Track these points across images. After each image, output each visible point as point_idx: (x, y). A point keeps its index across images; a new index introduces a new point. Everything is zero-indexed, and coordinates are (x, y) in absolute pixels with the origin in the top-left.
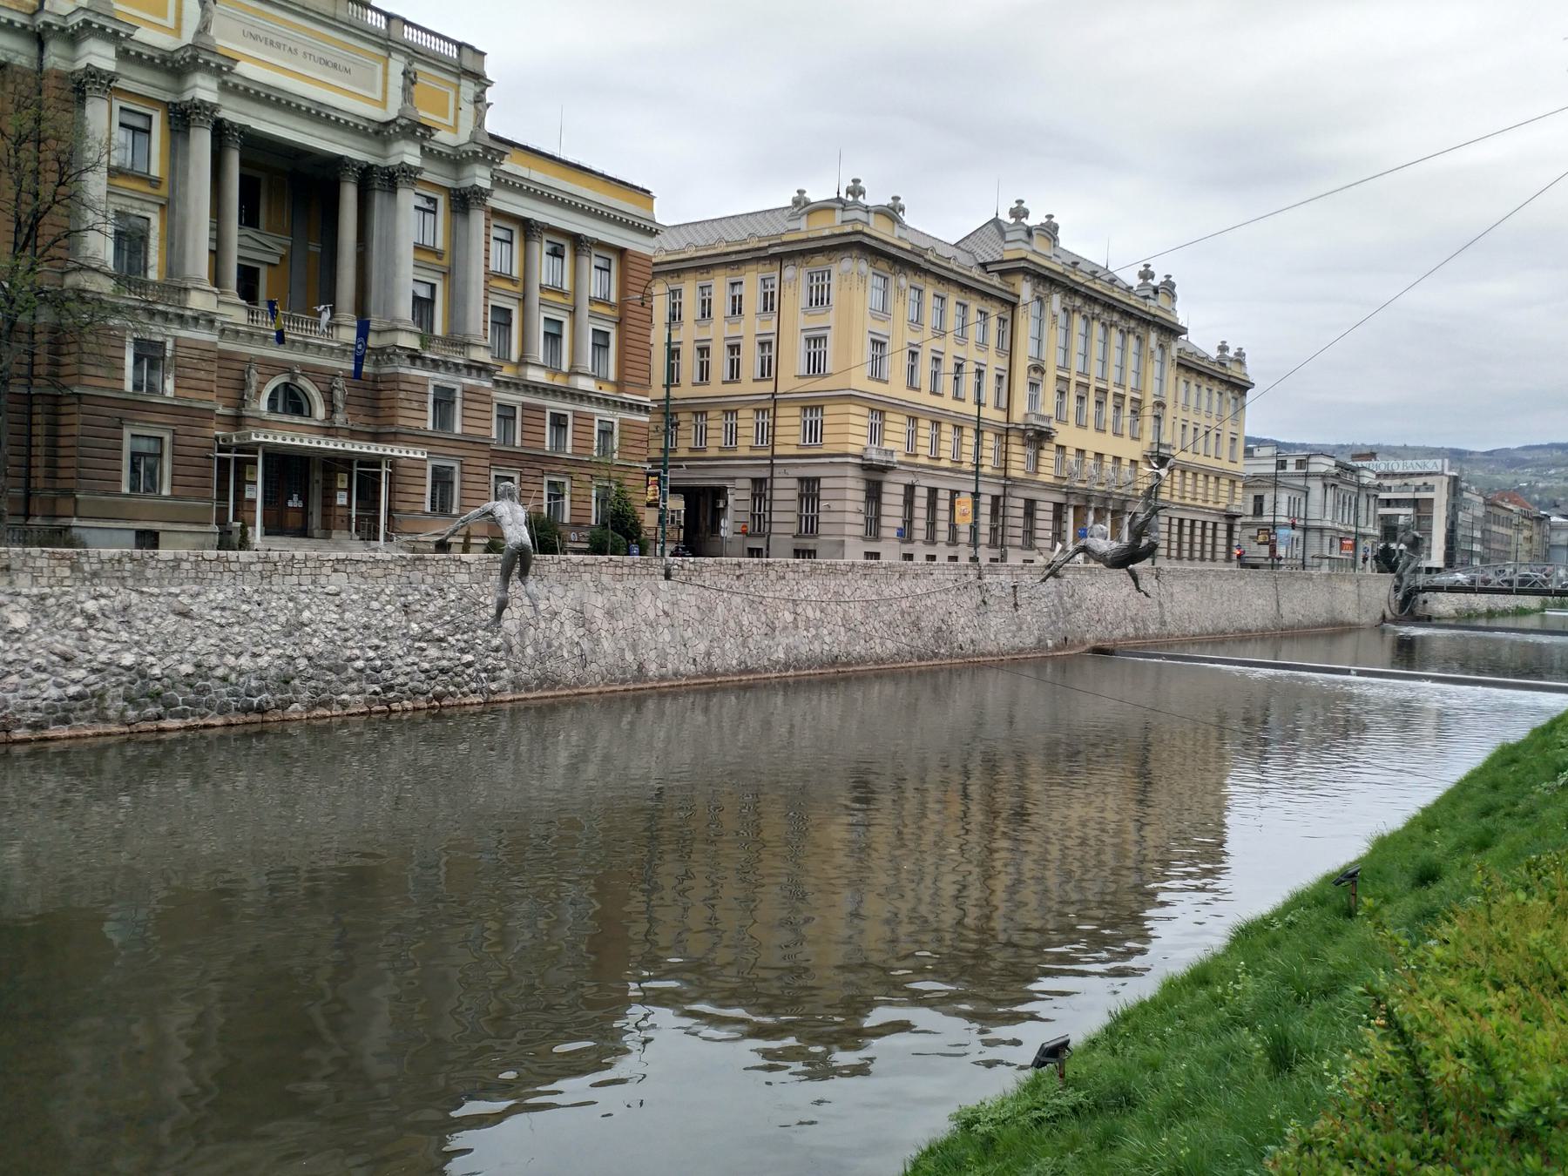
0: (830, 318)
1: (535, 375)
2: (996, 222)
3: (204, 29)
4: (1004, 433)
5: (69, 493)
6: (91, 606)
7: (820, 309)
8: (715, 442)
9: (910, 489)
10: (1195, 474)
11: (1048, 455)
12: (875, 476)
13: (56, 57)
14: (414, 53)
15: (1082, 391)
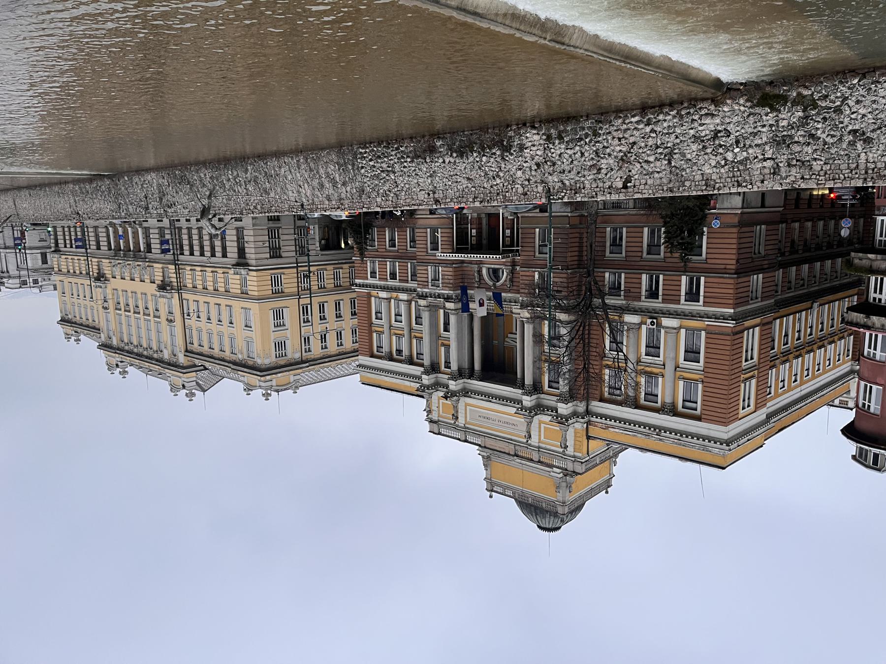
0: (273, 336)
1: (403, 296)
2: (204, 391)
3: (529, 424)
4: (180, 289)
5: (572, 227)
6: (498, 181)
7: (279, 340)
8: (328, 273)
9: (224, 255)
10: (81, 273)
11: (159, 278)
12: (243, 261)
13: (581, 407)
14: (455, 427)
15: (147, 312)
